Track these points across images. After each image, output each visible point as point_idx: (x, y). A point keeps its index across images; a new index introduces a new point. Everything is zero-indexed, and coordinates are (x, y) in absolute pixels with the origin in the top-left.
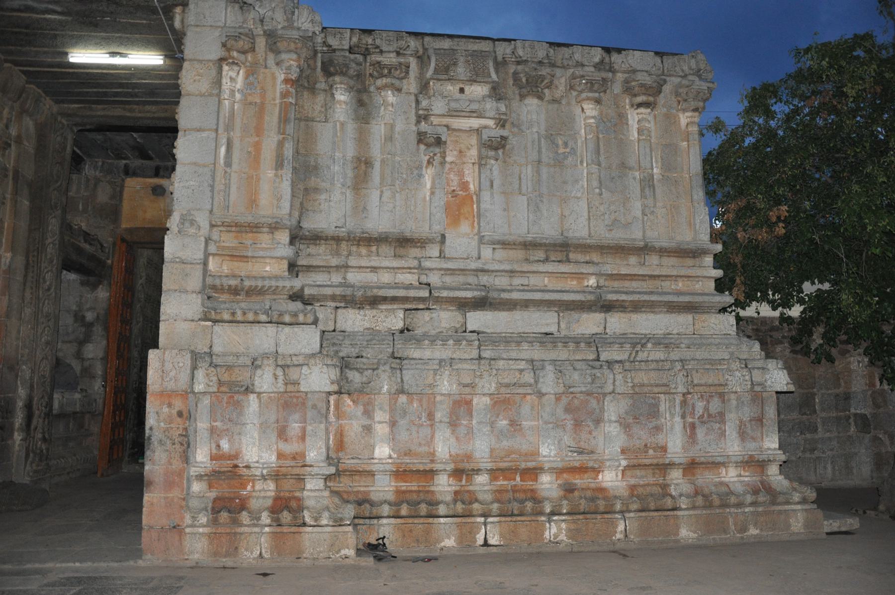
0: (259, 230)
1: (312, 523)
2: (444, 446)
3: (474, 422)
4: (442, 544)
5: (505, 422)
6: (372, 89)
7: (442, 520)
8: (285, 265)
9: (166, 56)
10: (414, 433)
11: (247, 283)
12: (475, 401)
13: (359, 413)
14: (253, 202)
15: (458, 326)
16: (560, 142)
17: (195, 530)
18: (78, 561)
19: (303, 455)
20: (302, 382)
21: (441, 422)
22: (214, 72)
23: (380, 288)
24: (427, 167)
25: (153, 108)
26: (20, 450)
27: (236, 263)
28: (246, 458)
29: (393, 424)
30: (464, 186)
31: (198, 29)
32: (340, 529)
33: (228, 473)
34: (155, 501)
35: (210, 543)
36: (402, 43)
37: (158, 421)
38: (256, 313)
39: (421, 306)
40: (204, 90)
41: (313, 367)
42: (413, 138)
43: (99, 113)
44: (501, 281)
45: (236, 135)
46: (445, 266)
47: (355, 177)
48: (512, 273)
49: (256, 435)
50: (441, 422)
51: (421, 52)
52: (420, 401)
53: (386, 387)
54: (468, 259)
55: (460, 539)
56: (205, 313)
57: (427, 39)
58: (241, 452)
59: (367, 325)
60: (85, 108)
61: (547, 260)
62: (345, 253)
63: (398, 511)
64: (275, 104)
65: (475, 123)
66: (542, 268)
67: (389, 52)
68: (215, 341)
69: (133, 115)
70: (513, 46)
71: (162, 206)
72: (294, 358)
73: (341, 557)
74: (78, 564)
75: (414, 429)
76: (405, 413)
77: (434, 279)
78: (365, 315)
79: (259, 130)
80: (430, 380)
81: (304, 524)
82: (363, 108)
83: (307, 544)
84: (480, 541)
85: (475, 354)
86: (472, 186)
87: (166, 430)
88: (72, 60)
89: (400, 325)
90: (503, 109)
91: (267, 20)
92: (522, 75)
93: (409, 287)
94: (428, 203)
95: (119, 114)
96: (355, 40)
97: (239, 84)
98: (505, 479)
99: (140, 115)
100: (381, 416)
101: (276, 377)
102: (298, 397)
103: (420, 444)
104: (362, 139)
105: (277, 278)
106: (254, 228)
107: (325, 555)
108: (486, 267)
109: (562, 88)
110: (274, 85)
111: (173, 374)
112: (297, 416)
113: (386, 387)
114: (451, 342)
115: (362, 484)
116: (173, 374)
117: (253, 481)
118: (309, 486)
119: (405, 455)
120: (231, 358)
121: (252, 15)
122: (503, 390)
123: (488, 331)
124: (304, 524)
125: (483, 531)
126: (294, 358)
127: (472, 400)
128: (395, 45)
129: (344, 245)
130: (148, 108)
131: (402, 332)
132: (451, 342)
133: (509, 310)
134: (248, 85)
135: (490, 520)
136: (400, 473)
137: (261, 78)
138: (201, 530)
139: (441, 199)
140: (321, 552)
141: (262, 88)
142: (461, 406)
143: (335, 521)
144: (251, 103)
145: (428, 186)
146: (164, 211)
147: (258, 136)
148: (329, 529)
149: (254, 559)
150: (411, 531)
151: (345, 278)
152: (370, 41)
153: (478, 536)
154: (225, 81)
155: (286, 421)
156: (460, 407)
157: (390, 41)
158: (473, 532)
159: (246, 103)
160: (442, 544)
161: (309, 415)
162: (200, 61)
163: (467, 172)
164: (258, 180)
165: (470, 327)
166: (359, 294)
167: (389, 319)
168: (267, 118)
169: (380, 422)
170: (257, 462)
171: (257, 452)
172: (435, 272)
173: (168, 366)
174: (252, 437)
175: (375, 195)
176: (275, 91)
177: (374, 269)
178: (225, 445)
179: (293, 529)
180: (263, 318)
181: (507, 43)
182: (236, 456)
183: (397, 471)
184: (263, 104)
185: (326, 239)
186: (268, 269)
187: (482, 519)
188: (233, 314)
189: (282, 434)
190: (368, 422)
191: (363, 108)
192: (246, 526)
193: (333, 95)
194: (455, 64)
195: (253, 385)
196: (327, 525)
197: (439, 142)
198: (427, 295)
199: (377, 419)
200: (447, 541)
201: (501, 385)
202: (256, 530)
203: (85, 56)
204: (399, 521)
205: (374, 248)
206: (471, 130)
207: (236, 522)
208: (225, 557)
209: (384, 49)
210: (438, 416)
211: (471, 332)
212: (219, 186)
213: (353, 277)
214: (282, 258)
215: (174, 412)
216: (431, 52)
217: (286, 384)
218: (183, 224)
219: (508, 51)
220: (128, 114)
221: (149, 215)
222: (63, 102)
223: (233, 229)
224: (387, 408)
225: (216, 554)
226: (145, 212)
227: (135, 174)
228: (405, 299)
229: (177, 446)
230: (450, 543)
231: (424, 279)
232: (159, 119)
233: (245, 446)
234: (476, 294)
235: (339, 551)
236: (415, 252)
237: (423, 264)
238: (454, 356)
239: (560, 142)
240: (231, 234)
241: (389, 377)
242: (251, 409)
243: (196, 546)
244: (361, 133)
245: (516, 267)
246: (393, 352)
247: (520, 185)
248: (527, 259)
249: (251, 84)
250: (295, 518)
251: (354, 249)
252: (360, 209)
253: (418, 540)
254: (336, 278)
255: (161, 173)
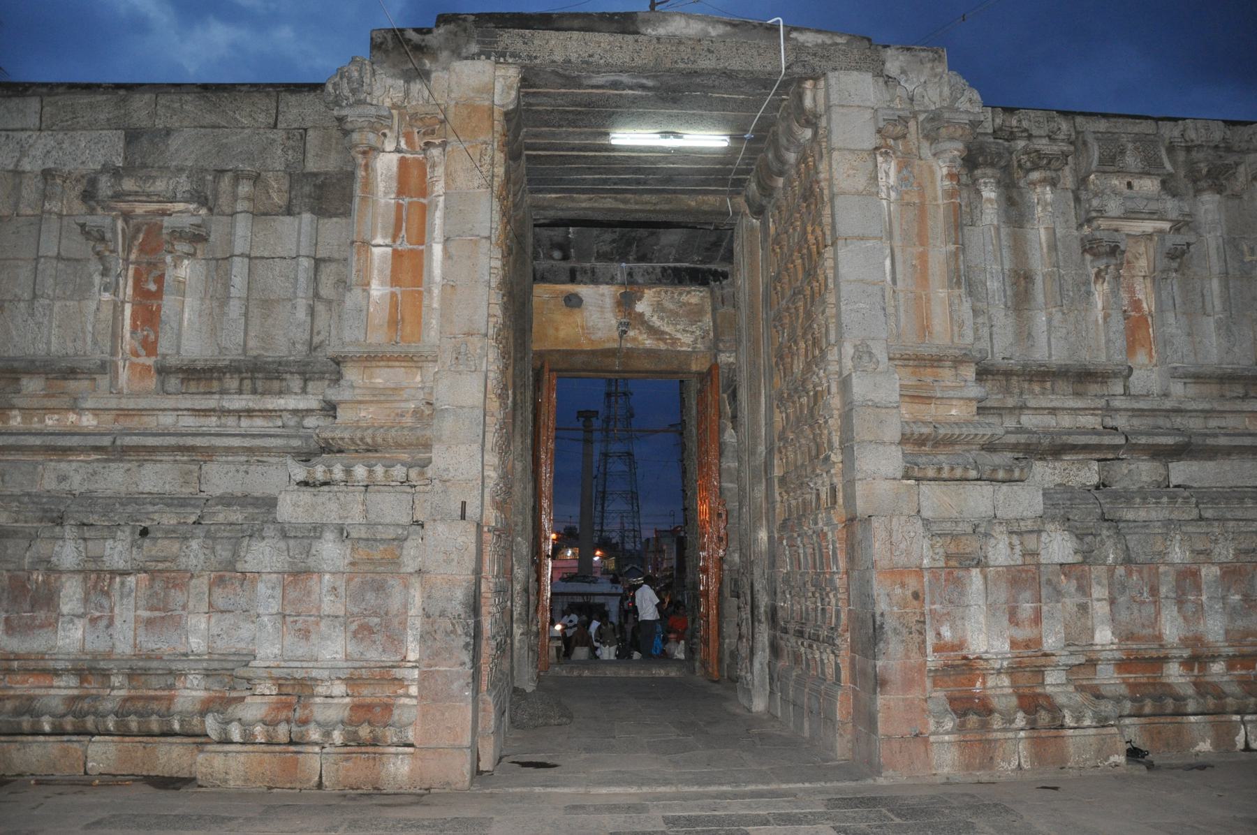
0: (941, 364)
1: (1072, 725)
2: (1171, 628)
3: (1204, 598)
4: (1197, 748)
5: (1237, 597)
6: (1022, 183)
7: (1192, 719)
8: (974, 406)
9: (732, 137)
10: (1136, 611)
11: (942, 431)
12: (1204, 571)
13: (1073, 590)
14: (925, 329)
15: (1161, 479)
16: (1245, 248)
17: (940, 738)
18: (807, 781)
19: (1038, 642)
20: (1042, 552)
21: (1167, 597)
22: (870, 165)
23: (1069, 434)
24: (1095, 283)
25: (654, 198)
26: (521, 648)
27: (916, 406)
28: (972, 648)
29: (1112, 602)
30: (1136, 304)
31: (844, 110)
32: (1105, 731)
33: (963, 667)
34: (892, 704)
35: (962, 754)
36: (1053, 125)
37: (890, 605)
38: (966, 469)
39: (1110, 456)
40: (861, 188)
41: (1053, 535)
42: (1076, 247)
43: (584, 205)
44: (1195, 424)
45: (897, 243)
46: (1136, 406)
47: (1016, 295)
48: (1207, 413)
49: (982, 619)
50: (1167, 597)
51: (1073, 137)
52: (1140, 572)
53: (1111, 556)
54: (1148, 395)
55: (1216, 745)
56: (907, 470)
57: (1079, 119)
58: (965, 641)
59: (1058, 480)
60: (591, 199)
61: (1245, 397)
62: (1017, 390)
63: (1142, 707)
64: (938, 206)
65: (1148, 226)
66: (1239, 405)
67: (1041, 137)
68: (924, 504)
69: (628, 207)
70: (1181, 127)
71: (579, 321)
72: (1022, 523)
73: (1110, 765)
74: (807, 785)
75: (1135, 607)
76: (1124, 587)
77: (1121, 422)
78: (1055, 468)
79: (922, 238)
80: (1159, 547)
81: (1062, 727)
82: (1015, 210)
83: (1071, 750)
84: (1240, 744)
85: (1194, 514)
86: (1145, 305)
87: (901, 616)
88: (613, 142)
89: (1095, 479)
90: (1187, 209)
91: (917, 98)
92: (1202, 165)
93: (1094, 432)
94: (1101, 328)
95: (609, 206)
96: (998, 121)
97: (892, 180)
98: (1243, 668)
99: (637, 207)
100: (1099, 592)
101: (1012, 547)
102: (1027, 571)
103: (1143, 626)
104: (1019, 247)
105: (967, 423)
106: (935, 361)
107: (1092, 763)
108: (1183, 406)
109: (1242, 179)
110: (933, 182)
111: (903, 546)
112: (1027, 594)
113: (1111, 556)
114: (1165, 500)
115: (1081, 676)
116: (903, 546)
117: (984, 676)
118: (1049, 680)
119: (1127, 639)
120: (949, 524)
121: (899, 91)
122: (1242, 557)
123: (1195, 485)
124: (1062, 727)
125: (1243, 732)
126: (1022, 523)
127: (1199, 570)
128: (1046, 128)
129: (1014, 380)
130: (646, 197)
131: (1097, 488)
132: (1165, 500)
133: (1210, 458)
134: (903, 180)
135: (1248, 718)
136: (1123, 665)
137: (916, 171)
138: (947, 738)
139: (1118, 324)
140: (1087, 759)
141: (920, 185)
142: (1188, 578)
143: (1099, 721)
144: (908, 204)
145: (1100, 306)
146: (583, 328)
147: (922, 245)
148: (1092, 731)
149: (1012, 771)
150: (1159, 733)
151: (1019, 422)
152: (1014, 123)
153: (1237, 738)
154: (881, 175)
155: (1016, 601)
156: (1184, 580)
157: (1039, 122)
158: (1232, 730)
159: (904, 204)
160: (1197, 748)
161: (1044, 592)
162: (852, 151)
163: (1138, 288)
164: (928, 300)
165: (1174, 481)
166: (1046, 441)
167: (1082, 473)
168: (930, 223)
169: (1098, 600)
170: (987, 652)
171: (986, 638)
172: (1122, 413)
173: (896, 537)
174: (978, 622)
175: (1041, 319)
176: (935, 189)
177: (1053, 411)
178: (946, 633)
179: (1053, 733)
180: (973, 474)
181: (1172, 123)
182: (961, 646)
183: (1128, 659)
184: (923, 204)
185: (998, 372)
186: (953, 412)
187: (1237, 718)
188: (940, 470)
189: (1013, 619)
190: (1084, 600)
191: (1015, 210)
192: (998, 730)
193: (978, 192)
194: (1123, 152)
195: (986, 557)
196: (1089, 727)
197: (1114, 251)
198: (1123, 442)
199: (1095, 596)
200: (1201, 744)
201: (1239, 552)
202: (1010, 735)
203: (630, 137)
204: (1143, 720)
205: (1048, 385)
206: (1149, 236)
207: (985, 726)
208: (979, 770)
209: (1034, 132)
210: (1163, 590)
211: (1176, 486)
212: (890, 310)
213: (1028, 420)
214: (970, 399)
215: (909, 593)
216: (1090, 138)
217: (1024, 555)
218: (860, 358)
219: (1176, 133)
220: (622, 206)
221: (562, 334)
222: (540, 191)
223: (911, 363)
224: (1105, 582)
225: (968, 767)
226: (557, 329)
227: (543, 279)
228: (1098, 448)
229: (915, 635)
230: (1205, 746)
231: (1109, 422)
232: (660, 211)
233: (969, 634)
234: (1179, 439)
235: (1107, 759)
236: (1094, 388)
237: (1111, 404)
238: (1173, 517)
239: (1245, 248)
240: (909, 370)
241: (1115, 544)
242: (974, 587)
243: (945, 758)
244: (1015, 240)
245: (1217, 406)
246: (1103, 513)
247: (1203, 302)
248: (1222, 396)
249: (907, 179)
250: (1054, 719)
251: (1026, 385)
252: (1024, 334)
253: (1168, 744)
254: (1010, 423)
255: (579, 277)
